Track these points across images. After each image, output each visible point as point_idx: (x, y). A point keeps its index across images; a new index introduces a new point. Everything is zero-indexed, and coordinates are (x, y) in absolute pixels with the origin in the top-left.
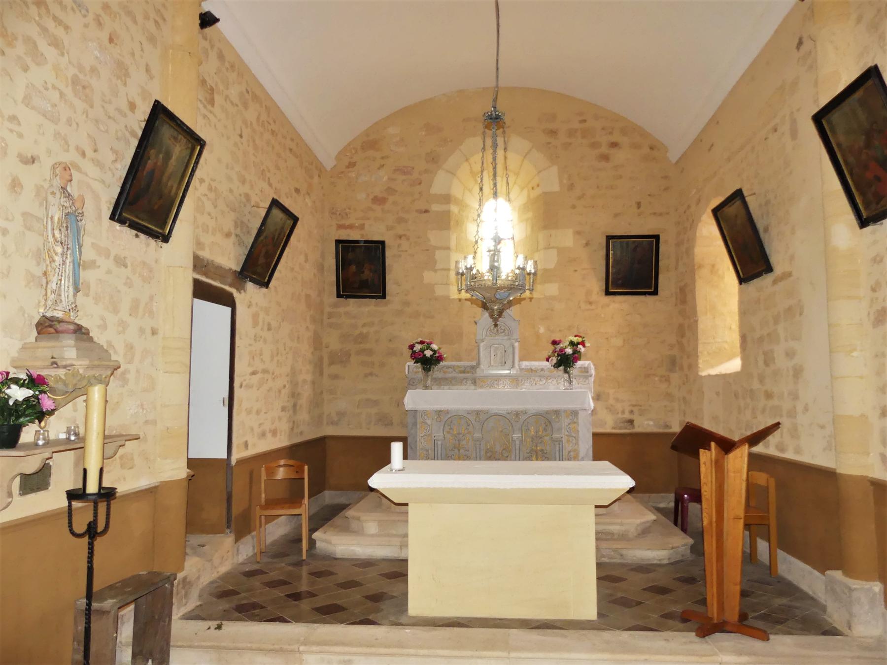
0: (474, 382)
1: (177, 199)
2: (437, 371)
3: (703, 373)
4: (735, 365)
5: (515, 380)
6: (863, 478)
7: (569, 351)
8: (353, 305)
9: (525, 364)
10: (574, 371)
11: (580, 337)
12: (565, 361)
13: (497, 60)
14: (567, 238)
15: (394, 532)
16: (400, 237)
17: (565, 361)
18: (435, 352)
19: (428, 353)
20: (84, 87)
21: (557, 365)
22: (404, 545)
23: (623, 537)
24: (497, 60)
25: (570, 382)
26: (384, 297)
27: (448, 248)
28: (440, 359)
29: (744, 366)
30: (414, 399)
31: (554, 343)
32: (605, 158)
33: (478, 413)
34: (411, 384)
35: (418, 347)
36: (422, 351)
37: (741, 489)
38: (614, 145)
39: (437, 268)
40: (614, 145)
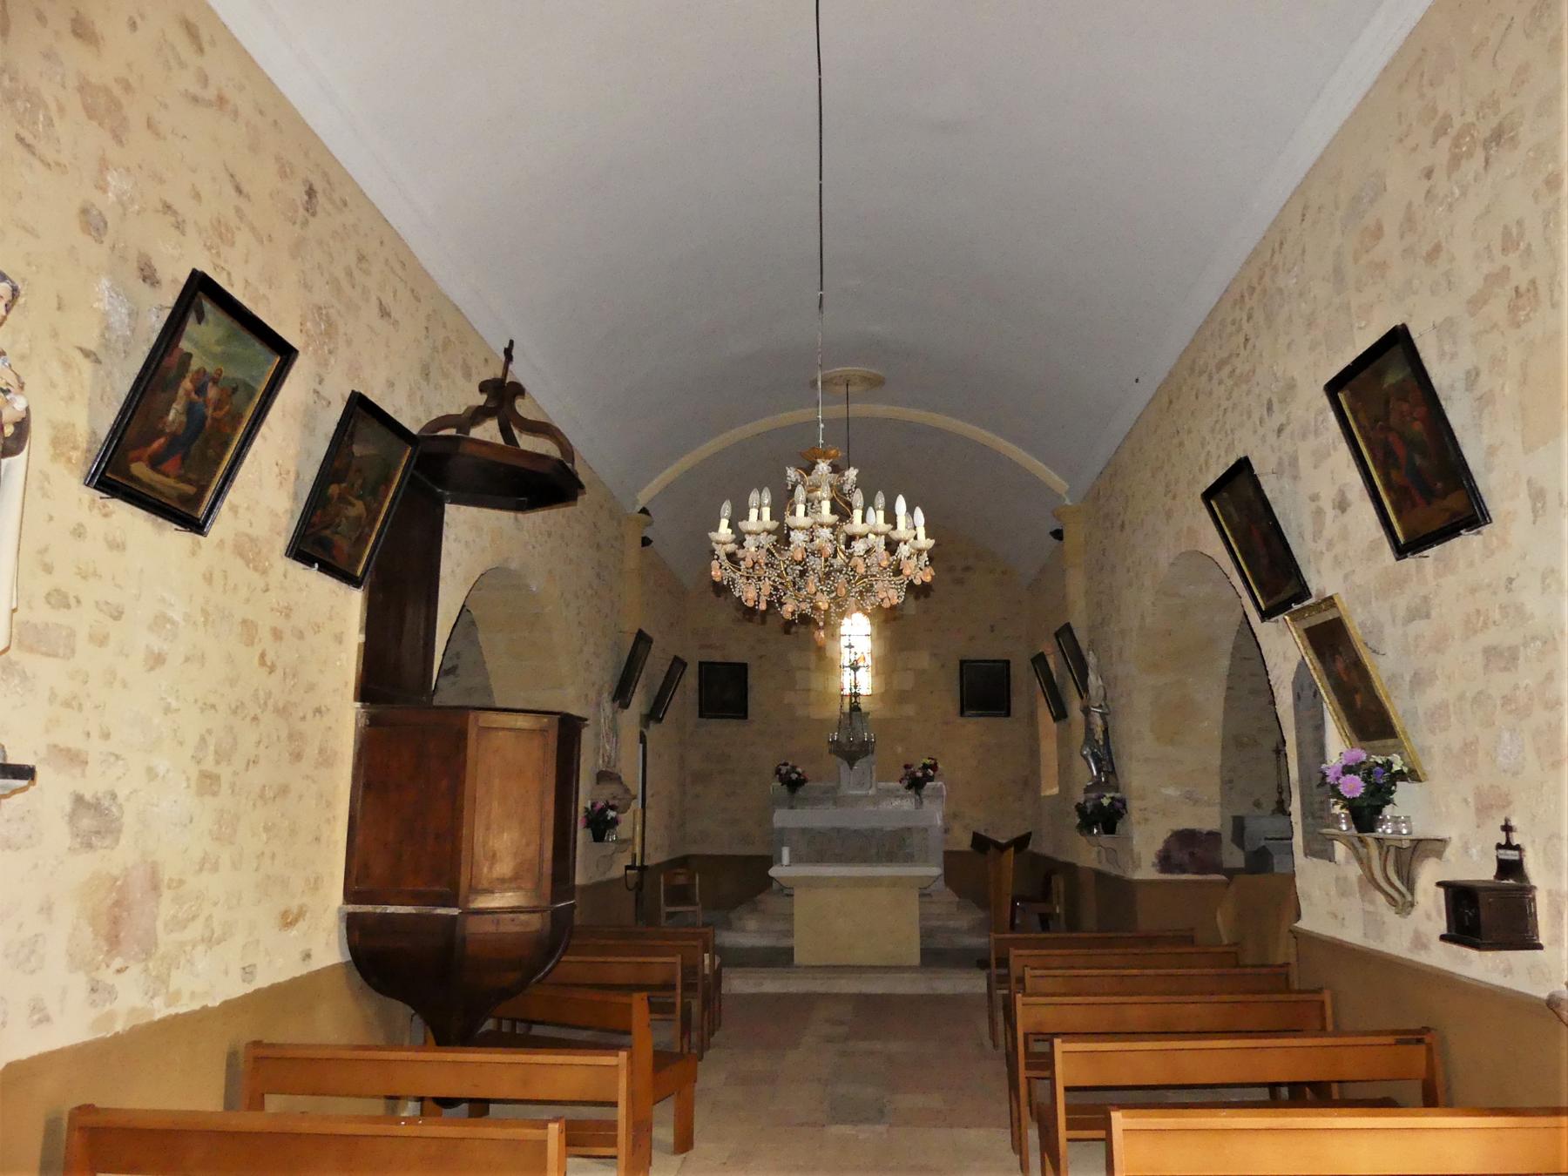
0: (835, 803)
1: (234, 435)
2: (801, 792)
3: (1043, 794)
4: (1055, 791)
5: (876, 800)
6: (1090, 868)
7: (919, 774)
8: (715, 725)
9: (882, 785)
10: (924, 792)
11: (933, 759)
12: (916, 784)
13: (820, 80)
14: (923, 660)
15: (1313, 423)
16: (761, 657)
17: (916, 784)
18: (799, 774)
19: (794, 776)
20: (142, 270)
21: (909, 787)
22: (789, 933)
23: (956, 931)
24: (820, 80)
25: (922, 803)
26: (745, 717)
27: (808, 669)
28: (805, 781)
29: (1060, 791)
30: (783, 818)
31: (907, 767)
32: (960, 582)
33: (839, 830)
34: (777, 803)
35: (784, 770)
36: (788, 773)
37: (1218, 975)
38: (967, 569)
39: (797, 687)
40: (967, 569)
